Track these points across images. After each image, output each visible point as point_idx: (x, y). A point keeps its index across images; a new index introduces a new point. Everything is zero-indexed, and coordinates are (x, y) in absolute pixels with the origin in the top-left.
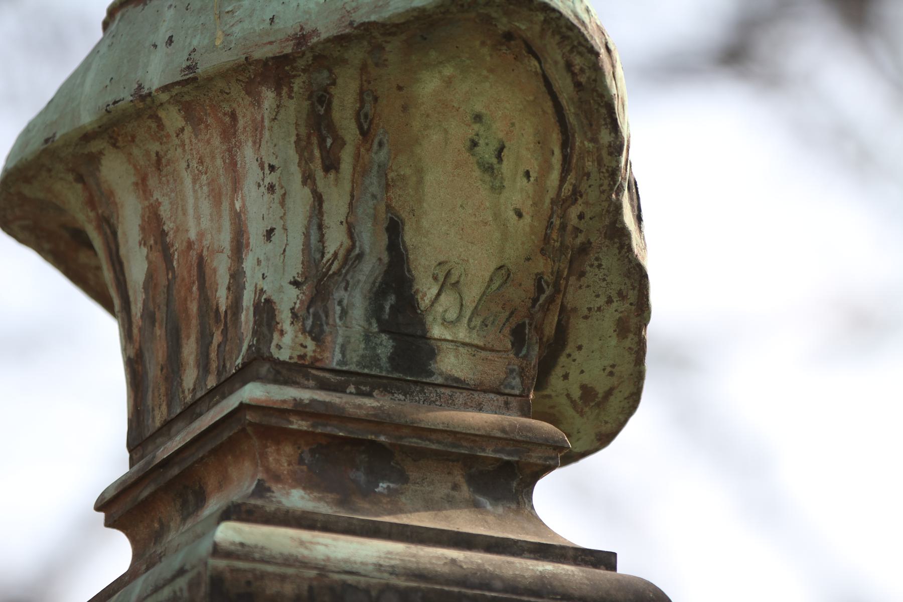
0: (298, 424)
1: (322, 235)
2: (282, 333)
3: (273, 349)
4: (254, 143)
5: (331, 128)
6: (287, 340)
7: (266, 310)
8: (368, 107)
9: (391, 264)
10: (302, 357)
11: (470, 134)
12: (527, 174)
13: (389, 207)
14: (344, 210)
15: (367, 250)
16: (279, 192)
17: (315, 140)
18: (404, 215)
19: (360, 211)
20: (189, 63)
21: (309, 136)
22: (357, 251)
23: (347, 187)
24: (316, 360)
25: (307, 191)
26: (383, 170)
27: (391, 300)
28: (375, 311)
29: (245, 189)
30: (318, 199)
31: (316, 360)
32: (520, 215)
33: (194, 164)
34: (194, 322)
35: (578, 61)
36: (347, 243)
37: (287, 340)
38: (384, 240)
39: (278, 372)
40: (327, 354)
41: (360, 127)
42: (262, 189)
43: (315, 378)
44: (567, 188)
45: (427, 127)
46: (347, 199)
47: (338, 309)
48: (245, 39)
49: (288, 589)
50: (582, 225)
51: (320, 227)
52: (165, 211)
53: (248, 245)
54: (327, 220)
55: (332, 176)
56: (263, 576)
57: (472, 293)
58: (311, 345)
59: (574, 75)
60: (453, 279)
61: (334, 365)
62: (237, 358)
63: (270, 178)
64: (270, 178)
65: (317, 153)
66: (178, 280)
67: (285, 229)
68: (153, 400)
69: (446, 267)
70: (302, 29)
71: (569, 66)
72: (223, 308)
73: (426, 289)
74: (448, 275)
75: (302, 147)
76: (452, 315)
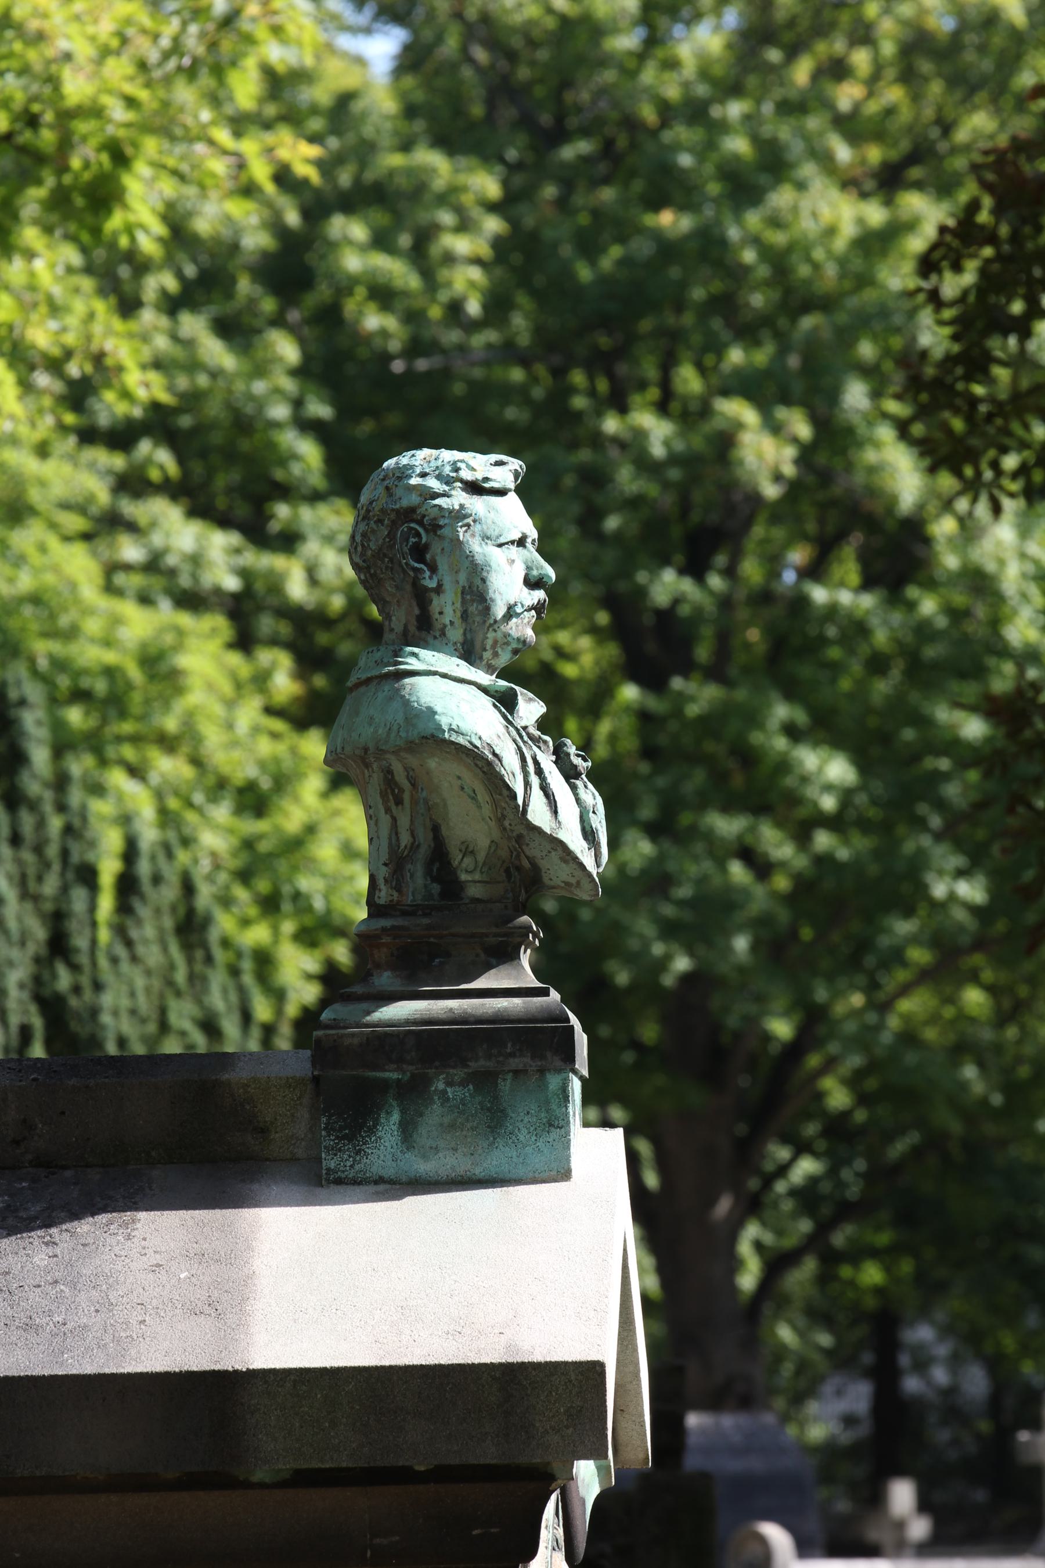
0: (385, 940)
2: (380, 890)
5: (396, 784)
6: (383, 894)
8: (411, 773)
15: (422, 841)
16: (374, 819)
23: (408, 811)
24: (398, 902)
25: (388, 816)
26: (426, 801)
27: (436, 867)
28: (428, 872)
30: (394, 819)
36: (411, 840)
37: (383, 894)
38: (431, 835)
41: (410, 782)
44: (499, 815)
46: (409, 818)
49: (356, 1041)
51: (397, 834)
54: (399, 830)
55: (400, 807)
56: (342, 1036)
57: (481, 857)
58: (396, 894)
65: (391, 797)
67: (378, 837)
73: (456, 858)
74: (467, 847)
75: (383, 795)
76: (471, 867)
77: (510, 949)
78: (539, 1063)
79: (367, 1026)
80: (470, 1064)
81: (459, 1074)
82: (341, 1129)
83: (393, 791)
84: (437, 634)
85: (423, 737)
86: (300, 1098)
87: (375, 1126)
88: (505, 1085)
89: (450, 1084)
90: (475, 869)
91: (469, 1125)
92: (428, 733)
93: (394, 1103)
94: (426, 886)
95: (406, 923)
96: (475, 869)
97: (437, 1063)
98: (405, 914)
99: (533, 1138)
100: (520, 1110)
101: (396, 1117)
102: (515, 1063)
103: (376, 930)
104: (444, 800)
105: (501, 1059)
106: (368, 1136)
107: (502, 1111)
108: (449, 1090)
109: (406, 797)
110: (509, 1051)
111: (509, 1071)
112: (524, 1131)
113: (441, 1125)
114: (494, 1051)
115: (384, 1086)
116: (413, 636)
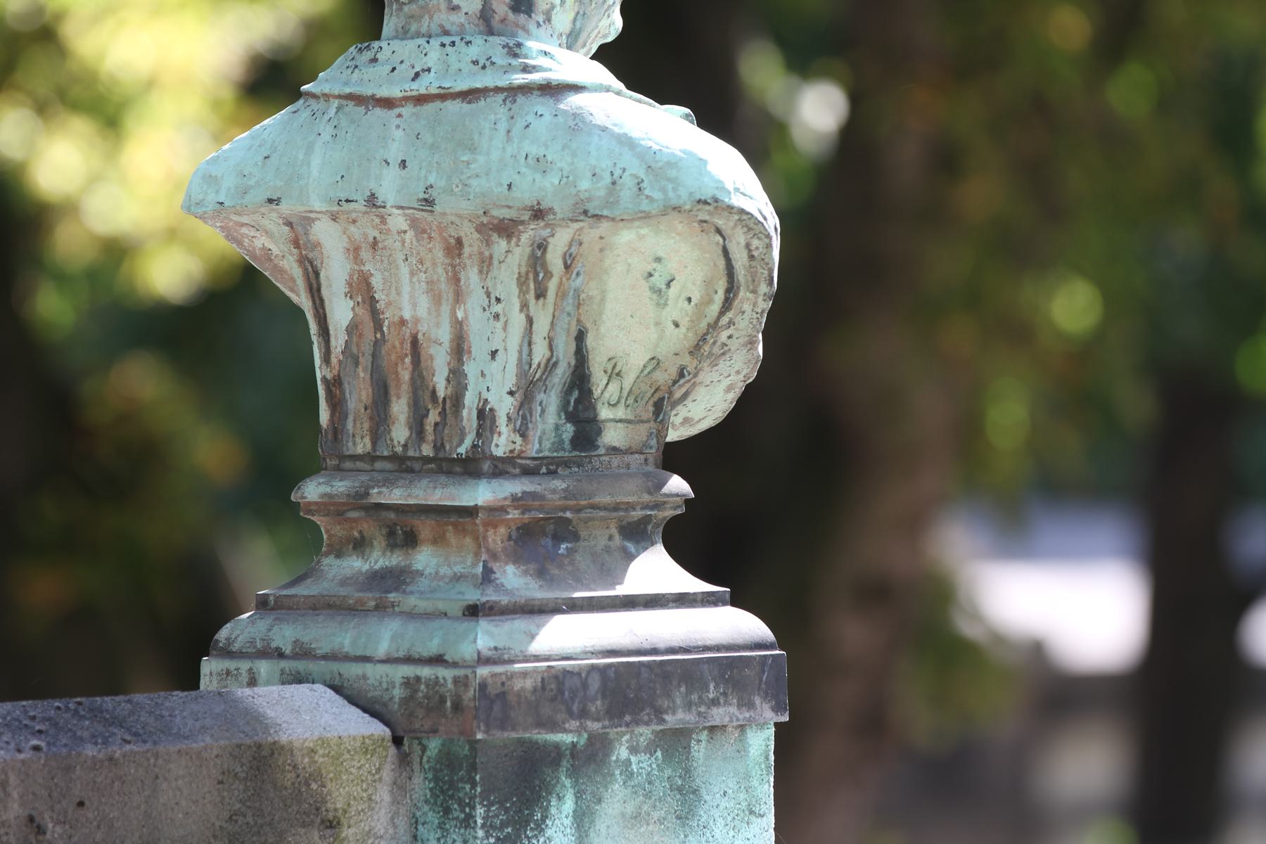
1: (531, 350)
3: (493, 448)
4: (481, 272)
7: (485, 416)
9: (576, 367)
10: (511, 451)
11: (649, 268)
12: (689, 300)
13: (579, 321)
14: (547, 327)
17: (531, 276)
18: (588, 325)
19: (558, 328)
20: (426, 196)
21: (527, 273)
22: (554, 359)
26: (577, 292)
27: (576, 394)
29: (469, 305)
30: (530, 321)
31: (522, 452)
32: (677, 325)
33: (413, 260)
34: (405, 387)
35: (755, 243)
36: (548, 354)
39: (496, 466)
40: (529, 446)
42: (487, 313)
43: (521, 466)
45: (616, 262)
47: (539, 408)
48: (483, 194)
49: (529, 684)
50: (728, 342)
51: (530, 344)
52: (377, 281)
53: (470, 352)
55: (541, 301)
56: (511, 676)
57: (628, 382)
58: (519, 440)
59: (750, 251)
60: (617, 370)
61: (534, 455)
62: (459, 445)
63: (498, 308)
64: (498, 308)
65: (532, 286)
66: (389, 345)
68: (354, 426)
69: (613, 362)
70: (539, 203)
71: (748, 246)
72: (441, 393)
73: (598, 379)
75: (522, 282)
77: (650, 527)
78: (747, 715)
79: (537, 658)
80: (666, 717)
81: (645, 733)
82: (503, 825)
83: (536, 274)
84: (541, 19)
85: (699, 201)
86: (378, 770)
87: (544, 818)
88: (700, 749)
89: (634, 750)
90: (618, 402)
91: (656, 815)
92: (706, 194)
93: (568, 782)
94: (557, 428)
95: (538, 488)
96: (618, 402)
97: (628, 718)
98: (528, 472)
99: (731, 833)
100: (716, 790)
101: (569, 805)
102: (719, 715)
103: (505, 499)
104: (603, 293)
105: (702, 709)
106: (536, 836)
107: (695, 792)
108: (633, 759)
109: (552, 286)
110: (711, 696)
111: (705, 728)
112: (721, 822)
113: (623, 815)
114: (694, 697)
115: (554, 755)
116: (503, 21)
